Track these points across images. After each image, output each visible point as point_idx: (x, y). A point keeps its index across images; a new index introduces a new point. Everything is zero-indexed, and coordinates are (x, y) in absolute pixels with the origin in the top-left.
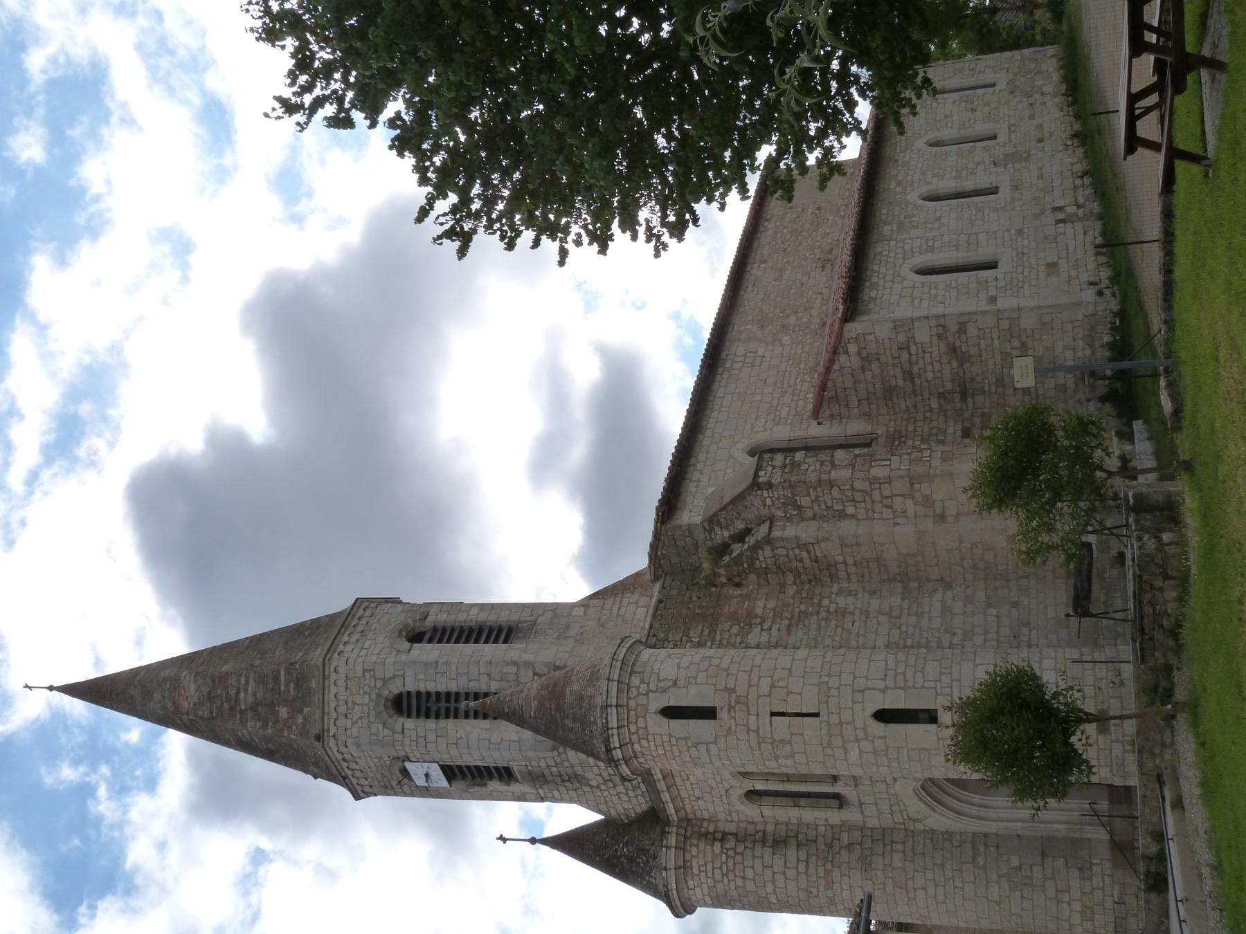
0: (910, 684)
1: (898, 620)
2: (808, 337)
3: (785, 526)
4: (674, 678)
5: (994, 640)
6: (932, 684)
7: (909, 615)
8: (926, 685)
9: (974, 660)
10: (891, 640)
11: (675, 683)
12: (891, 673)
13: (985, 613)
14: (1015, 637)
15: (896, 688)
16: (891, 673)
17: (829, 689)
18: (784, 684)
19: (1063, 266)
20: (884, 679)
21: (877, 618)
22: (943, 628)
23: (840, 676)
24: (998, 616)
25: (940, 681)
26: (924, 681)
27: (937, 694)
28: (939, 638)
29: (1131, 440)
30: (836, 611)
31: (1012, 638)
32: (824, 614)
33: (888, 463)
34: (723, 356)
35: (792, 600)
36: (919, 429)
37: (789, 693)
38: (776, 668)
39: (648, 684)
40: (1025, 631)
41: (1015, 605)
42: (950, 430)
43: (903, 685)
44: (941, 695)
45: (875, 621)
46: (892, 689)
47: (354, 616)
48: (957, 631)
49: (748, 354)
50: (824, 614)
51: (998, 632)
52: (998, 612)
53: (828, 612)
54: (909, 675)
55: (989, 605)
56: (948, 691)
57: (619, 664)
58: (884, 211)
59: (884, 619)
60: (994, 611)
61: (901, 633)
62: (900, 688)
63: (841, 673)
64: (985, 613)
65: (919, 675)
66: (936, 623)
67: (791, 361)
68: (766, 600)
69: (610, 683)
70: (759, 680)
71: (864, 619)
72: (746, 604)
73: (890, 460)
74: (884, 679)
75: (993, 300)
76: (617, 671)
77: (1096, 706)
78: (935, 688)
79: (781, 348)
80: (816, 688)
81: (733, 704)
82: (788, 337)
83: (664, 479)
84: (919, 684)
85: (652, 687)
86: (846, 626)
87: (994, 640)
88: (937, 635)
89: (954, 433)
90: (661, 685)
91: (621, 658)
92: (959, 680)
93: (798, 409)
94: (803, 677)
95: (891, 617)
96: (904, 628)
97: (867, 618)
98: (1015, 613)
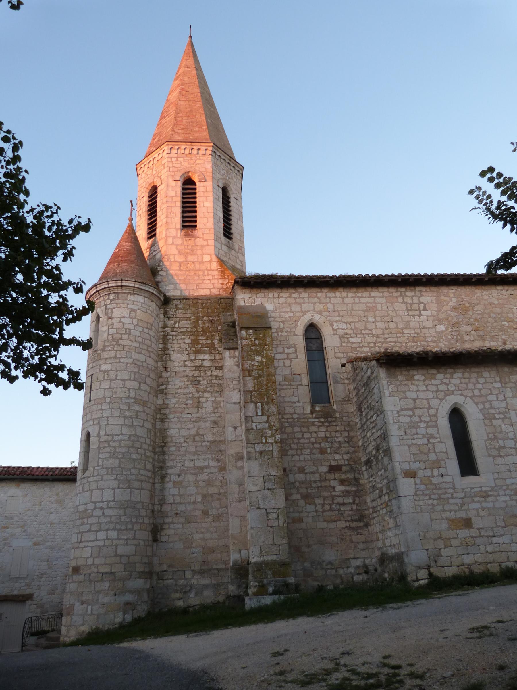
0: (101, 451)
1: (192, 440)
2: (446, 343)
3: (234, 358)
4: (113, 316)
5: (174, 500)
6: (100, 463)
7: (196, 447)
8: (100, 460)
9: (119, 488)
10: (174, 438)
11: (109, 318)
12: (110, 438)
13: (198, 494)
14: (176, 514)
15: (100, 442)
16: (110, 438)
17: (101, 404)
18: (106, 378)
19: (464, 533)
20: (106, 435)
21: (194, 427)
22: (185, 469)
23: (109, 408)
24: (195, 502)
25: (103, 468)
26: (103, 459)
27: (94, 467)
28: (176, 467)
29: (275, 593)
30: (199, 402)
31: (175, 512)
32: (197, 395)
33: (260, 413)
34: (418, 289)
35: (209, 375)
36: (338, 434)
37: (100, 381)
38: (117, 371)
39: (111, 304)
40: (182, 520)
41: (205, 513)
42: (337, 457)
43: (101, 446)
44: (94, 470)
45: (191, 426)
46: (99, 440)
47: (217, 150)
48: (181, 478)
49: (492, 315)
50: (197, 395)
51: (181, 503)
52: (198, 502)
53: (199, 398)
54: (108, 449)
55: (204, 496)
56: (96, 474)
57: (120, 284)
58: (366, 349)
59: (193, 431)
60: (199, 500)
61: (181, 443)
62: (99, 445)
63: (111, 409)
64: (198, 494)
65: (107, 455)
66: (188, 464)
67: (416, 335)
68: (210, 360)
69: (106, 283)
70: (109, 363)
71: (193, 420)
72: (206, 349)
73: (262, 415)
74: (106, 435)
75: (411, 474)
76: (114, 285)
77: (82, 565)
78: (98, 466)
79: (431, 326)
80: (102, 396)
81: (98, 352)
82: (444, 329)
83: (256, 272)
84: (100, 456)
85: (108, 307)
86: (186, 409)
87: (174, 500)
88: (178, 465)
89: (335, 460)
90: (109, 311)
91: (124, 284)
92: (102, 480)
93: (358, 349)
94: (110, 388)
95: (194, 436)
96: (184, 444)
97: (194, 422)
98: (198, 513)
